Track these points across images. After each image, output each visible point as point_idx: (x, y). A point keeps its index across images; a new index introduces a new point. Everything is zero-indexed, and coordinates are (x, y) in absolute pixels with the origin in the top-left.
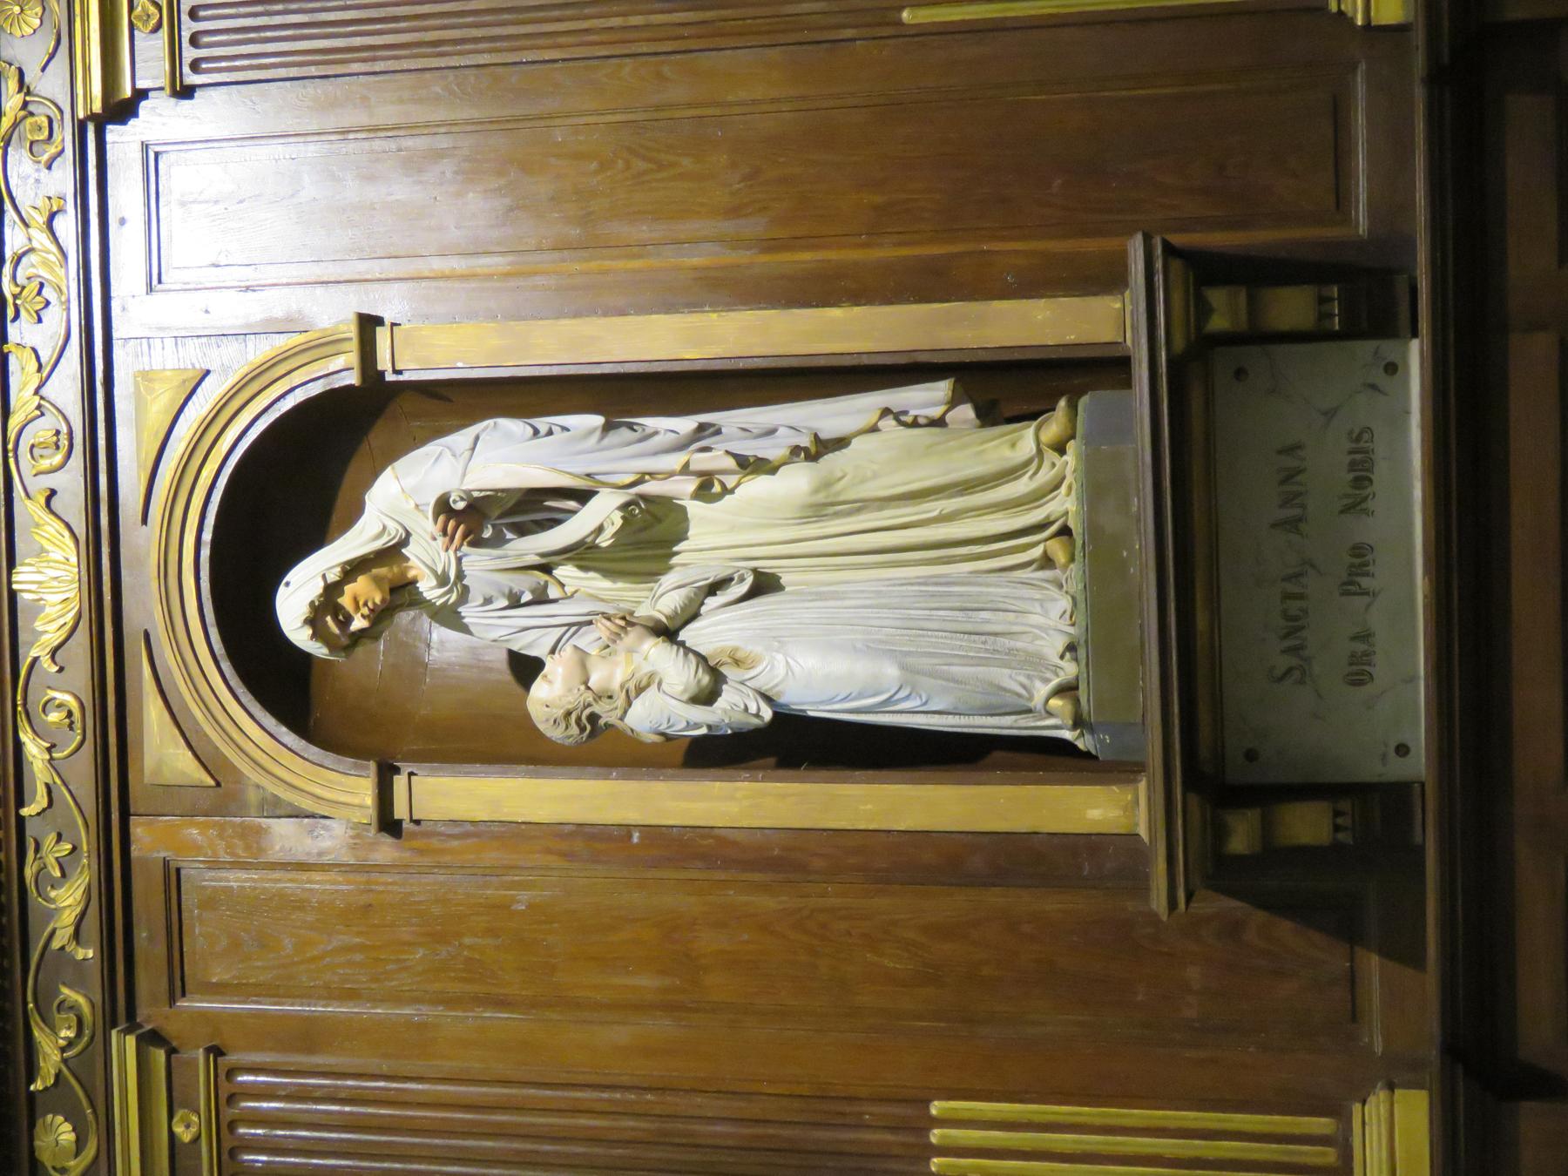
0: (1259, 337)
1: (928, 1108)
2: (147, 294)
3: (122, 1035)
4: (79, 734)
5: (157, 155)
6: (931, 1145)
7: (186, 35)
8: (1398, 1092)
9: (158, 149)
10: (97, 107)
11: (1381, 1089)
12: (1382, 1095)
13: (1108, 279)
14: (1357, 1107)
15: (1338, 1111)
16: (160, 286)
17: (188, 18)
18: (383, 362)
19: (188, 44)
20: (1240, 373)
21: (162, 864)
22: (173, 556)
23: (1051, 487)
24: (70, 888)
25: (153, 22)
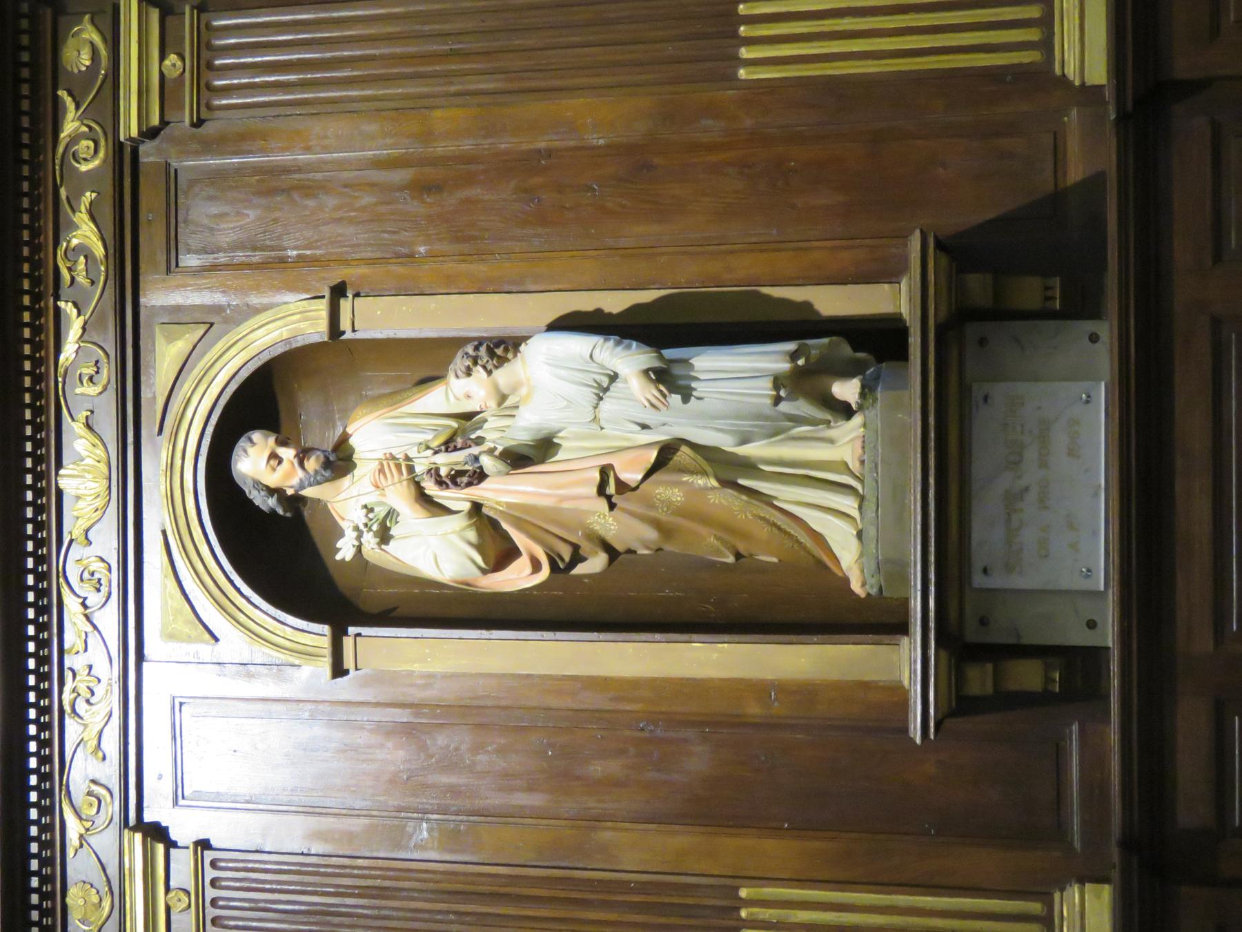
0: (1000, 313)
1: (738, 892)
2: (174, 807)
3: (132, 833)
4: (102, 74)
5: (181, 704)
6: (741, 899)
7: (208, 900)
8: (1087, 885)
9: (183, 700)
10: (134, 132)
11: (1075, 883)
12: (1076, 888)
13: (886, 273)
14: (1057, 896)
15: (1046, 898)
16: (177, 270)
17: (205, 109)
18: (345, 324)
19: (209, 866)
20: (982, 342)
21: (165, 165)
22: (178, 462)
23: (848, 519)
24: (94, 248)
25: (184, 905)
